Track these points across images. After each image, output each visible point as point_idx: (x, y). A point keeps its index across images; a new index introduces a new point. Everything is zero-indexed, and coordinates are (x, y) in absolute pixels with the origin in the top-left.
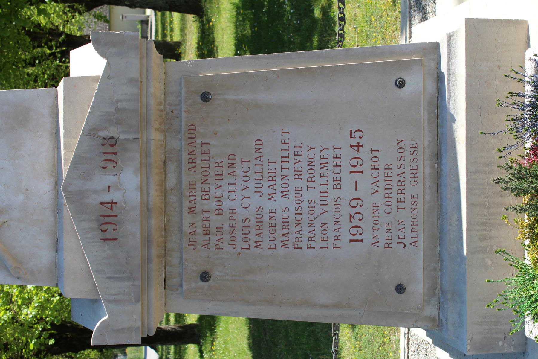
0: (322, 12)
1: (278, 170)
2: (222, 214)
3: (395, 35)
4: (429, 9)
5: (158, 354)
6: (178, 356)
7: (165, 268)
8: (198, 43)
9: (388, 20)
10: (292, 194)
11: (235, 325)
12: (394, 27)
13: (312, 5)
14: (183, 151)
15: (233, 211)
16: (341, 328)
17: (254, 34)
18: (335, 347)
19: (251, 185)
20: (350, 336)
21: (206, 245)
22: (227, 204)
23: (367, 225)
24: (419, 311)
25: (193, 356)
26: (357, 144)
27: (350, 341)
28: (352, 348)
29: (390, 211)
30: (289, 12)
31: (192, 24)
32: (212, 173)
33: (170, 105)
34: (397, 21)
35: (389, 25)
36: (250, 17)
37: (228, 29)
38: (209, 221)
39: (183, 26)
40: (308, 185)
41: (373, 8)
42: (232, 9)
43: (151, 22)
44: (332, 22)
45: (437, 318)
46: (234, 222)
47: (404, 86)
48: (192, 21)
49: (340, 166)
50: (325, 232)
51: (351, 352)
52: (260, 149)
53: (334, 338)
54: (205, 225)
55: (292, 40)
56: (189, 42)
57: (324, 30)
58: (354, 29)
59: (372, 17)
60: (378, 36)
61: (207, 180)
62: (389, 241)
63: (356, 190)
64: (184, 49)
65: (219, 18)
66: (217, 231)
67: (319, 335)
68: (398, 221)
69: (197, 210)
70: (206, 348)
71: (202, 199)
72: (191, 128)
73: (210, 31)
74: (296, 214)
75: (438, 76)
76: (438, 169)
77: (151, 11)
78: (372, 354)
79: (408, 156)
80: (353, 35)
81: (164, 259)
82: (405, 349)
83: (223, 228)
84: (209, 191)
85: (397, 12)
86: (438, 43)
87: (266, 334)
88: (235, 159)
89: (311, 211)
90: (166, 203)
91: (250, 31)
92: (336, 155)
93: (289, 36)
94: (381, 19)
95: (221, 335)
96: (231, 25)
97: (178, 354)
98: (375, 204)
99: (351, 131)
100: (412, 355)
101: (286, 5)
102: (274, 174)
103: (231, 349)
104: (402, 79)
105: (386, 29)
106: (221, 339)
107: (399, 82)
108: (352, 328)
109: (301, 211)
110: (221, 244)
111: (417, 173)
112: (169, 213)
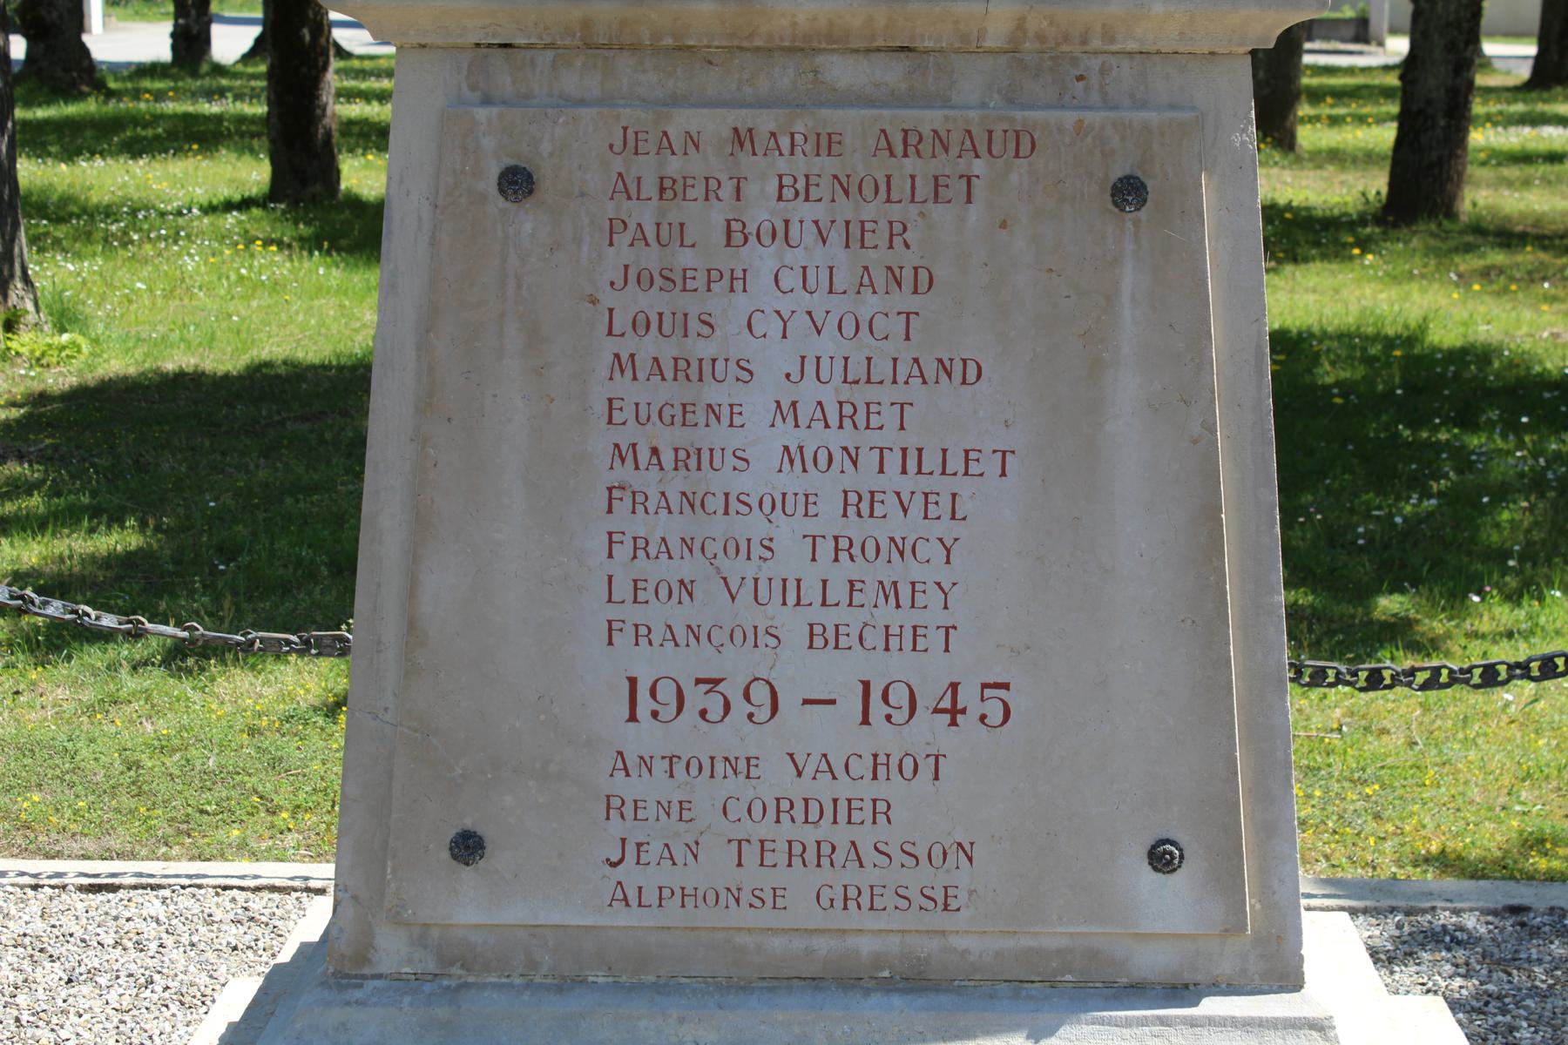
0: (1393, 620)
1: (876, 438)
2: (728, 244)
3: (1317, 861)
4: (1405, 974)
5: (237, 62)
6: (228, 129)
7: (547, 47)
8: (1289, 207)
9: (1367, 838)
10: (792, 482)
11: (335, 319)
12: (1344, 860)
13: (1417, 588)
14: (946, 112)
15: (738, 281)
16: (324, 663)
17: (1319, 393)
18: (262, 640)
19: (828, 345)
20: (298, 698)
21: (625, 188)
22: (762, 260)
23: (685, 735)
24: (390, 910)
25: (228, 176)
26: (960, 706)
27: (282, 697)
28: (256, 703)
29: (732, 816)
30: (1394, 511)
31: (1354, 191)
32: (868, 211)
33: (1104, 71)
34: (1363, 868)
35: (1349, 842)
36: (1379, 380)
37: (1339, 308)
38: (707, 199)
39: (1349, 160)
40: (824, 537)
41: (1408, 789)
42: (1406, 320)
43: (1360, 53)
44: (1362, 652)
45: (366, 971)
46: (700, 283)
47: (1155, 869)
48: (1366, 186)
49: (887, 649)
50: (663, 593)
51: (244, 701)
52: (949, 375)
53: (294, 638)
54: (693, 186)
55: (1301, 520)
56: (1294, 177)
57: (1334, 626)
58: (1335, 726)
59: (1377, 787)
60: (1313, 806)
61: (847, 193)
62: (628, 810)
63: (806, 702)
64: (1271, 162)
65: (1376, 278)
66: (670, 224)
67: (302, 595)
68: (697, 843)
69: (744, 158)
70: (257, 220)
71: (781, 177)
72: (1022, 143)
73: (1331, 246)
74: (727, 495)
75: (1186, 986)
76: (874, 982)
77: (1399, 54)
78: (238, 769)
79: (917, 879)
80: (1317, 721)
81: (577, 42)
82: (256, 877)
83: (682, 245)
84: (807, 199)
85: (1394, 869)
86: (1301, 987)
87: (304, 419)
88: (916, 292)
89: (738, 548)
90: (768, 51)
91: (1329, 380)
92: (925, 636)
93: (1312, 510)
94: (1370, 817)
95: (302, 274)
96: (1351, 320)
97: (236, 130)
98: (757, 766)
99: (1006, 686)
100: (233, 900)
101: (1420, 500)
102: (861, 422)
103: (254, 304)
104: (1180, 862)
105: (1335, 832)
106: (289, 271)
107: (1171, 853)
108: (327, 706)
109: (738, 513)
110: (627, 238)
111: (859, 907)
112: (737, 61)
